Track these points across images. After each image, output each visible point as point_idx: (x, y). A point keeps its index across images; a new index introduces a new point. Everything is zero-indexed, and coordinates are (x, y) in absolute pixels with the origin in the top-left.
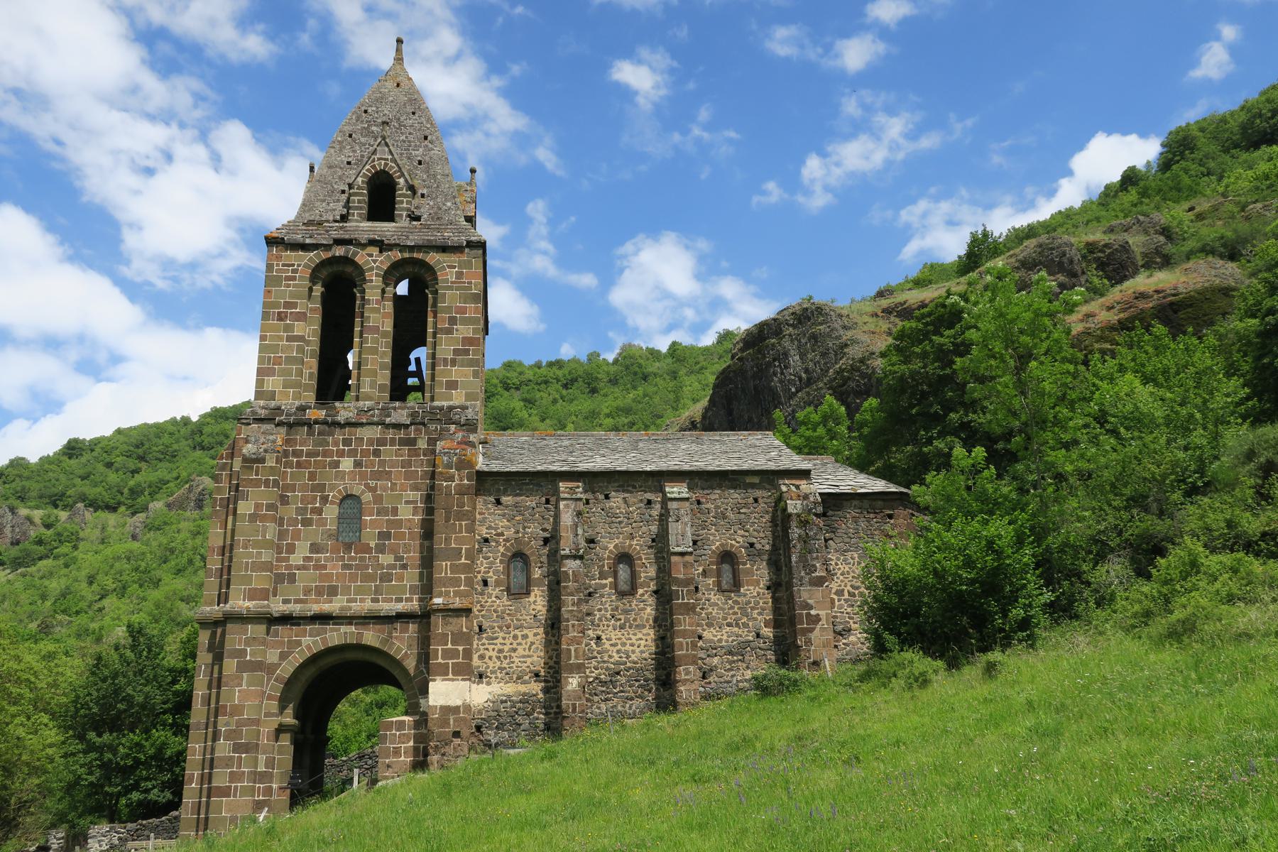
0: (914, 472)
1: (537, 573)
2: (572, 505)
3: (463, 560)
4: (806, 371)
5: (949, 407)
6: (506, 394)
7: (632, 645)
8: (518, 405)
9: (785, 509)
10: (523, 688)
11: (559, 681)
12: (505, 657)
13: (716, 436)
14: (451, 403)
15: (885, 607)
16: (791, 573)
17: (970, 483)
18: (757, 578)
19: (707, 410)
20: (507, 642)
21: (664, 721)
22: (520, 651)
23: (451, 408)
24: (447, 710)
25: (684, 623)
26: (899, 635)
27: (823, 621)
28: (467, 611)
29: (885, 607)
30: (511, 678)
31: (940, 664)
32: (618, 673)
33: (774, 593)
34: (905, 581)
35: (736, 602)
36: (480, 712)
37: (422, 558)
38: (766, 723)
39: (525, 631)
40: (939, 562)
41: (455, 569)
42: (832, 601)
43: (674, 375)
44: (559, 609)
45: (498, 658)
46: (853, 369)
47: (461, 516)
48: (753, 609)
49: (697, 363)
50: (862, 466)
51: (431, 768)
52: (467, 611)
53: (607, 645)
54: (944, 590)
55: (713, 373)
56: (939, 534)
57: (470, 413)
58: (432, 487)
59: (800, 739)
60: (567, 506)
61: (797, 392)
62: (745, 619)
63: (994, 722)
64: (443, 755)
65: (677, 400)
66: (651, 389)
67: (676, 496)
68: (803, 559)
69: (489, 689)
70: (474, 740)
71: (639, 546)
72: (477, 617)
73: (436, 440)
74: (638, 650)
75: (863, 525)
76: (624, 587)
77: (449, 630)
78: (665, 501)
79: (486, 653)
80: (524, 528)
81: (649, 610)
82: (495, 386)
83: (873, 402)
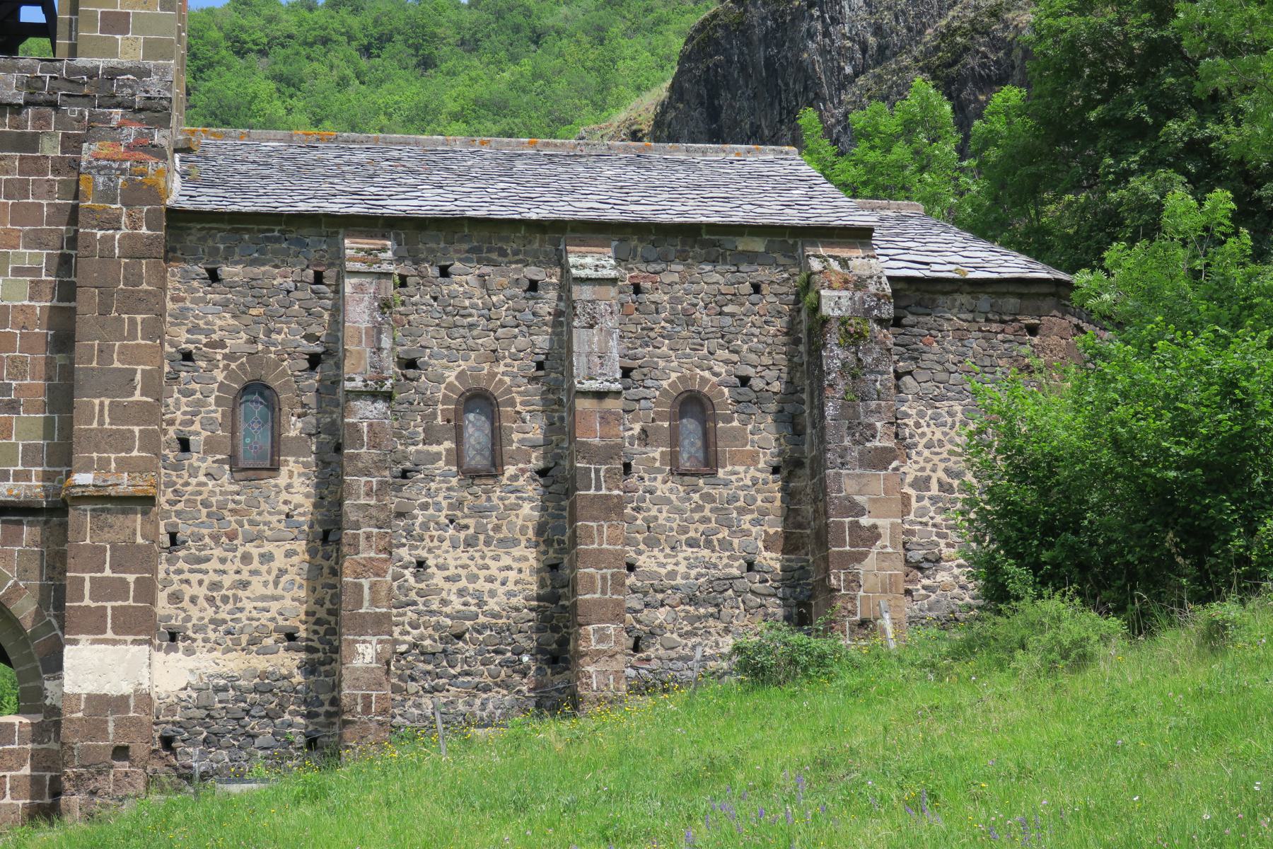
0: (1084, 252)
1: (294, 428)
2: (371, 285)
3: (137, 396)
4: (878, 30)
5: (1166, 108)
6: (238, 63)
7: (491, 580)
8: (266, 87)
9: (816, 309)
10: (261, 663)
11: (336, 650)
12: (225, 599)
13: (679, 152)
14: (114, 62)
15: (1010, 510)
16: (822, 439)
17: (1199, 264)
18: (756, 443)
19: (665, 107)
20: (228, 566)
21: (551, 731)
22: (257, 587)
23: (113, 73)
24: (102, 704)
25: (599, 536)
26: (1036, 567)
27: (885, 540)
28: (147, 501)
29: (1010, 510)
30: (237, 642)
31: (1114, 623)
32: (459, 637)
33: (786, 481)
34: (1053, 460)
35: (708, 498)
36: (170, 709)
37: (51, 390)
38: (758, 735)
39: (268, 547)
40: (1123, 423)
41: (120, 413)
42: (906, 499)
43: (599, 35)
44: (340, 504)
45: (210, 600)
46: (976, 29)
47: (134, 302)
48: (741, 511)
49: (649, 10)
50: (985, 227)
51: (67, 818)
52: (147, 501)
53: (438, 579)
54: (1130, 478)
55: (679, 33)
56: (1125, 366)
57: (154, 85)
58: (73, 241)
59: (824, 764)
60: (359, 289)
61: (856, 75)
62: (724, 533)
63: (1211, 732)
64: (93, 793)
65: (604, 88)
66: (549, 63)
67: (591, 273)
68: (848, 407)
69: (190, 662)
70: (157, 765)
71: (509, 377)
72: (166, 515)
73: (79, 140)
74: (501, 590)
75: (975, 344)
76: (475, 459)
77: (106, 540)
78: (567, 283)
79: (184, 589)
80: (269, 332)
81: (526, 509)
82: (215, 45)
83: (1011, 95)
